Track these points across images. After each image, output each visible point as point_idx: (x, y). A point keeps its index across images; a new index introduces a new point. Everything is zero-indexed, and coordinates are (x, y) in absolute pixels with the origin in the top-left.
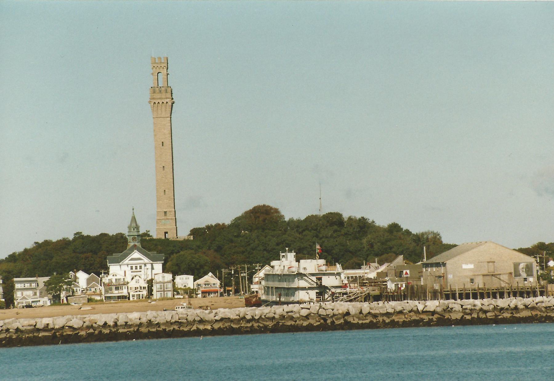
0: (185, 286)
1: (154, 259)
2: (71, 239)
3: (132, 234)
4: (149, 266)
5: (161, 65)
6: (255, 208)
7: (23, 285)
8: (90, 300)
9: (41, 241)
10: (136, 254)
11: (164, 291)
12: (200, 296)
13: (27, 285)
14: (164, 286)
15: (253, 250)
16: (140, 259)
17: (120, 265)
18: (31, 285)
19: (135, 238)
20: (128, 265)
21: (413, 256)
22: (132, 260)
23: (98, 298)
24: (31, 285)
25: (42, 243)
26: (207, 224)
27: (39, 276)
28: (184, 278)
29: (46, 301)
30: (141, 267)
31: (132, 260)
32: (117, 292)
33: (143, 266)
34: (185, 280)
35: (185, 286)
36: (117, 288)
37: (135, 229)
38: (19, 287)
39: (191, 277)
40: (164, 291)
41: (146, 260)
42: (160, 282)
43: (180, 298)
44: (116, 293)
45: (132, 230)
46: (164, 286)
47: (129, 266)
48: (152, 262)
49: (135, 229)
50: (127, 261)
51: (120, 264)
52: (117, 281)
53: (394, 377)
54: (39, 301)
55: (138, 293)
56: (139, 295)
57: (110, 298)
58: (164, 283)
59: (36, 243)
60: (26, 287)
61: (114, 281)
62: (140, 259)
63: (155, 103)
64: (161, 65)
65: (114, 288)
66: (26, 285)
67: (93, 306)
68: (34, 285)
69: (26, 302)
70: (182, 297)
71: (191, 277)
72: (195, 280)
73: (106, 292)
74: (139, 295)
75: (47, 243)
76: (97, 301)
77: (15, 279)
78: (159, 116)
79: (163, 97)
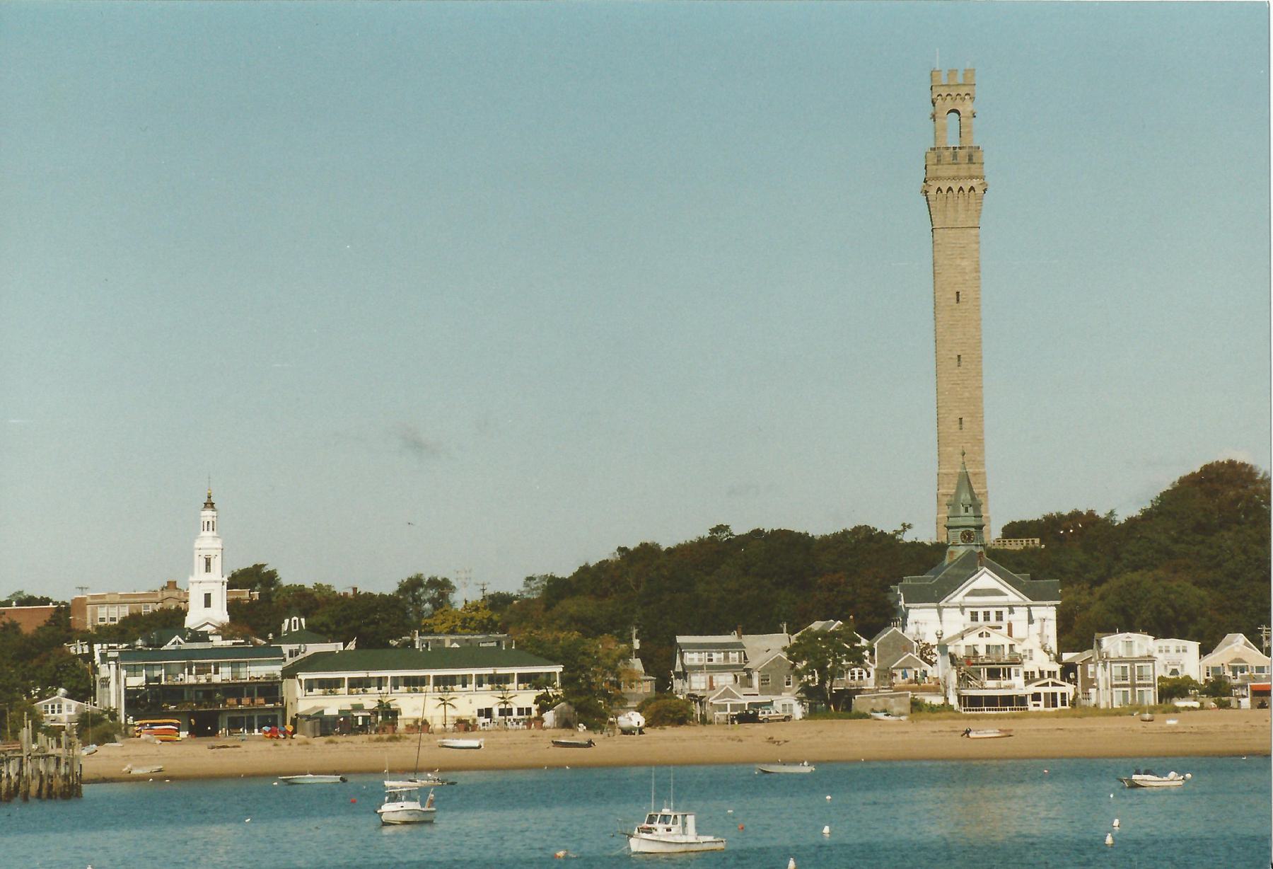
0: (1174, 672)
1: (1036, 595)
2: (664, 548)
3: (960, 522)
4: (1021, 614)
5: (949, 96)
6: (1207, 469)
7: (704, 656)
8: (916, 706)
9: (632, 545)
10: (986, 579)
11: (1133, 686)
12: (1246, 703)
13: (718, 657)
14: (1132, 670)
15: (1236, 579)
16: (996, 592)
17: (940, 610)
18: (726, 658)
19: (969, 534)
20: (962, 608)
21: (539, 644)
22: (974, 593)
23: (937, 700)
24: (726, 658)
25: (636, 550)
26: (1047, 513)
27: (746, 631)
28: (1173, 650)
29: (788, 702)
30: (999, 616)
31: (974, 593)
32: (992, 683)
33: (1005, 611)
34: (1173, 655)
35: (1174, 672)
36: (993, 674)
37: (971, 509)
38: (696, 662)
39: (1194, 646)
40: (1133, 686)
41: (1013, 596)
42: (1120, 660)
43: (1194, 708)
44: (991, 688)
45: (962, 512)
46: (1132, 670)
47: (968, 611)
48: (1029, 602)
49: (971, 509)
50: (959, 597)
51: (942, 604)
52: (993, 651)
53: (950, 858)
54: (771, 703)
55: (1050, 689)
56: (1054, 695)
57: (974, 702)
58: (1132, 661)
59: (621, 550)
60: (715, 662)
61: (982, 651)
62: (996, 592)
63: (939, 189)
64: (949, 96)
65: (984, 673)
66: (715, 656)
67: (1006, 724)
68: (734, 657)
69: (734, 707)
70: (1197, 704)
71: (1194, 646)
72: (1204, 651)
73: (964, 679)
74: (1054, 695)
75: (647, 552)
76: (933, 709)
77: (680, 639)
78: (950, 224)
79: (963, 173)
